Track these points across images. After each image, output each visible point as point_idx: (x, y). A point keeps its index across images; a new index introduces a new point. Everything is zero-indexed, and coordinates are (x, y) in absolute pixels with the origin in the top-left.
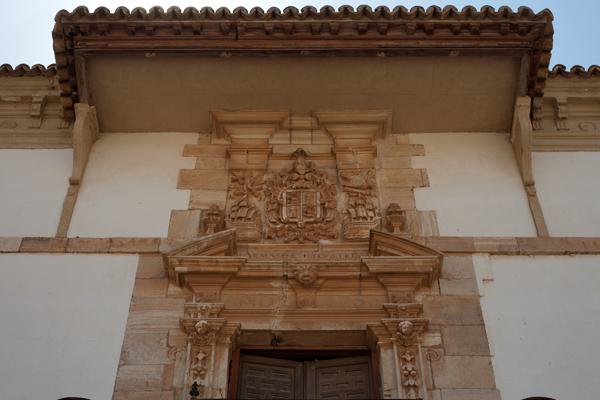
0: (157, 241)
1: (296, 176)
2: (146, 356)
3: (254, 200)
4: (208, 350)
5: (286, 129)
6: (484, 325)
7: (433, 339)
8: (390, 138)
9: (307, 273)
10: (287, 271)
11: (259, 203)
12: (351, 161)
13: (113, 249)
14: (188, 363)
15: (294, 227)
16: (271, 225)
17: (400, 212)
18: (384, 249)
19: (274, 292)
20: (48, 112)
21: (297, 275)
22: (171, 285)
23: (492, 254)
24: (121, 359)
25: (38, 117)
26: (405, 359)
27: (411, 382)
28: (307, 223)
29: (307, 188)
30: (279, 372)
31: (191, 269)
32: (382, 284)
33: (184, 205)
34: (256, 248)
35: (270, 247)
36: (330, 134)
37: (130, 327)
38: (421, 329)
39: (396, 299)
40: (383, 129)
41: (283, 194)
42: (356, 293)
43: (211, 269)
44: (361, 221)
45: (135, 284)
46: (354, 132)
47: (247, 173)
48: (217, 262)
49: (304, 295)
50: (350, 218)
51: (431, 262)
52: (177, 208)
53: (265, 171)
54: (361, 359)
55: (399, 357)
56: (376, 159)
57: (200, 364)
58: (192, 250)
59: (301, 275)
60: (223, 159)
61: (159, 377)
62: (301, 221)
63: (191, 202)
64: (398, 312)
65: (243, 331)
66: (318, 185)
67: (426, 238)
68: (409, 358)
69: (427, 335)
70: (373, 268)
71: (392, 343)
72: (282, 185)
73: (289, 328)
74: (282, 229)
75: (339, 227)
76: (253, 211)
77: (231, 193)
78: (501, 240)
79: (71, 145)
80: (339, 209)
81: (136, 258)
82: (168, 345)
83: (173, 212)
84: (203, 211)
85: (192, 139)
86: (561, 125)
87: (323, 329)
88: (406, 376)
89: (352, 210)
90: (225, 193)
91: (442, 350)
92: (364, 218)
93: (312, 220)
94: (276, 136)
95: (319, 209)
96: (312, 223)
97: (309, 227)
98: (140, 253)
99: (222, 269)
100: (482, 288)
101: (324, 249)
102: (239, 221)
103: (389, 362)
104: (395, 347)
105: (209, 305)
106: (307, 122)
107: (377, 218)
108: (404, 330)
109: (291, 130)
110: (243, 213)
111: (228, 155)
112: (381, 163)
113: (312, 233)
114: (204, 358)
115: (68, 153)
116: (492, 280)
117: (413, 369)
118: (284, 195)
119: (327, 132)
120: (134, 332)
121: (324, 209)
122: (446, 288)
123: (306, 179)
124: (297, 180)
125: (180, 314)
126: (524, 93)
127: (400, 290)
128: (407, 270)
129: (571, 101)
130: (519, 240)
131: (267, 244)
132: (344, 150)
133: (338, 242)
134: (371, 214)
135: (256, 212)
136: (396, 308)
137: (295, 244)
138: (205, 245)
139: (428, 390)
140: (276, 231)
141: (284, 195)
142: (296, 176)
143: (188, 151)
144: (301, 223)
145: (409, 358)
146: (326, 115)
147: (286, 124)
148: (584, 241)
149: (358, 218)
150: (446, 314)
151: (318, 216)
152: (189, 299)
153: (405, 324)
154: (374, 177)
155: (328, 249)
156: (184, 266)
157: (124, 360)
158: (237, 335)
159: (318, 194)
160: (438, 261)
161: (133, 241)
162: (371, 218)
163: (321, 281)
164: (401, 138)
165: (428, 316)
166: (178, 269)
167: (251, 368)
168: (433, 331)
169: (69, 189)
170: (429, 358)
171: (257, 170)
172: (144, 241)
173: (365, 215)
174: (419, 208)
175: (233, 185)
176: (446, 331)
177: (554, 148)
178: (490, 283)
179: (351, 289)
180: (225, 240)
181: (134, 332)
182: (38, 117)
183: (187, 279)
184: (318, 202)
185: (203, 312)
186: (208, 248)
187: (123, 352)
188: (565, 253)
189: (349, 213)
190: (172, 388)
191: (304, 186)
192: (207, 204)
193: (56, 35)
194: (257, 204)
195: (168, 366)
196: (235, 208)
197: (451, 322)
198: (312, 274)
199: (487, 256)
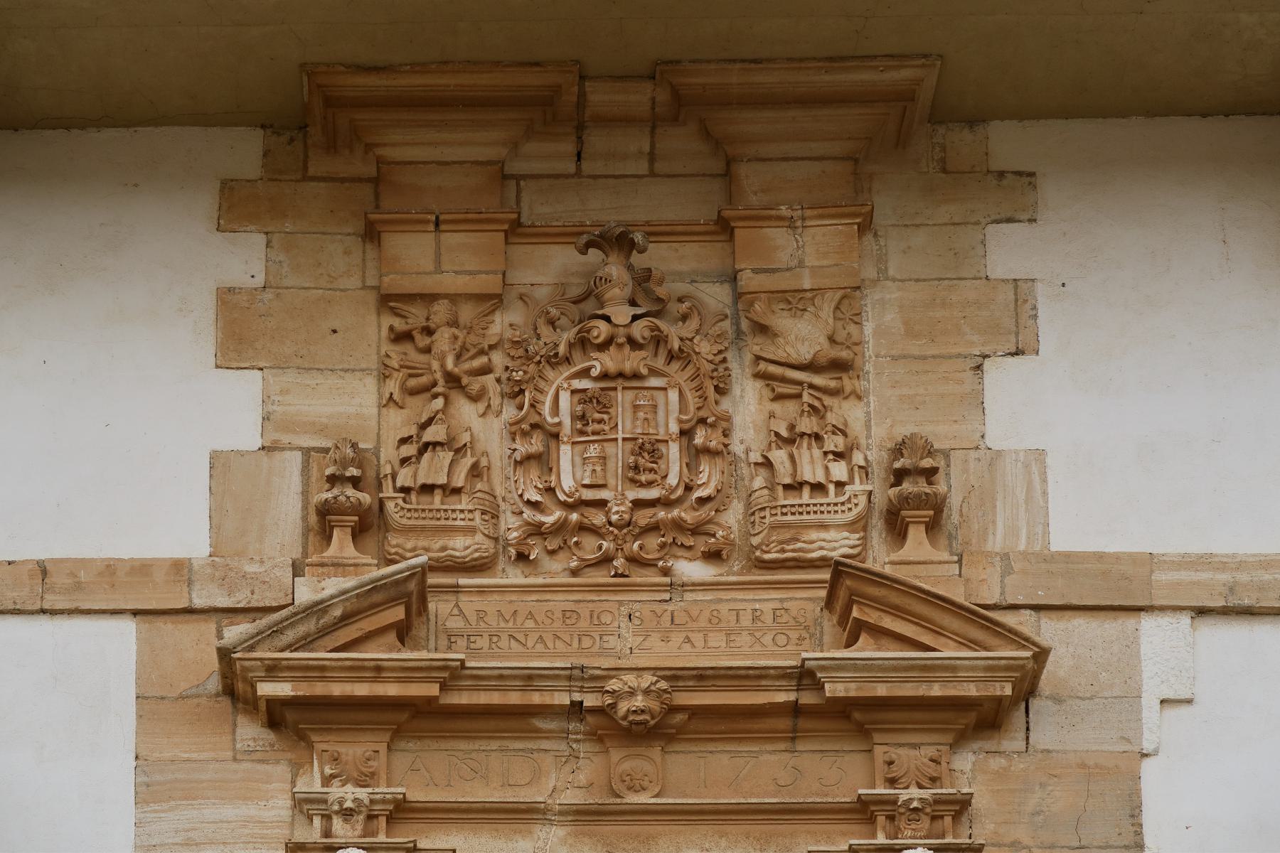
0: (180, 569)
3: (466, 412)
9: (639, 702)
15: (598, 518)
16: (528, 514)
17: (930, 474)
18: (872, 617)
19: (545, 744)
21: (613, 706)
22: (241, 719)
23: (1201, 612)
28: (638, 504)
29: (636, 376)
31: (304, 690)
34: (482, 591)
39: (895, 772)
44: (806, 496)
45: (139, 717)
47: (441, 311)
48: (379, 669)
50: (771, 487)
52: (225, 445)
53: (493, 301)
58: (301, 630)
59: (623, 707)
63: (266, 418)
67: (1005, 557)
72: (555, 361)
76: (468, 461)
77: (393, 386)
78: (1240, 564)
80: (737, 448)
81: (128, 627)
84: (307, 452)
89: (779, 456)
90: (371, 383)
92: (818, 488)
93: (653, 493)
94: (530, 147)
97: (643, 517)
98: (136, 613)
102: (425, 498)
105: (363, 794)
110: (434, 469)
113: (653, 541)
116: (1189, 702)
118: (565, 399)
119: (706, 134)
121: (695, 454)
125: (281, 807)
133: (732, 572)
134: (839, 470)
135: (475, 466)
136: (893, 801)
138: (337, 612)
140: (537, 530)
141: (565, 399)
144: (618, 511)
149: (795, 487)
151: (673, 480)
152: (297, 768)
154: (857, 319)
155: (700, 596)
156: (284, 679)
159: (673, 395)
162: (840, 485)
163: (679, 718)
166: (267, 689)
171: (412, 213)
172: (142, 569)
173: (820, 477)
175: (396, 354)
178: (1184, 710)
183: (290, 716)
184: (674, 428)
185: (347, 814)
186: (346, 619)
189: (767, 464)
191: (628, 367)
192: (322, 430)
194: (477, 424)
196: (408, 450)
198: (655, 705)
199: (1185, 620)
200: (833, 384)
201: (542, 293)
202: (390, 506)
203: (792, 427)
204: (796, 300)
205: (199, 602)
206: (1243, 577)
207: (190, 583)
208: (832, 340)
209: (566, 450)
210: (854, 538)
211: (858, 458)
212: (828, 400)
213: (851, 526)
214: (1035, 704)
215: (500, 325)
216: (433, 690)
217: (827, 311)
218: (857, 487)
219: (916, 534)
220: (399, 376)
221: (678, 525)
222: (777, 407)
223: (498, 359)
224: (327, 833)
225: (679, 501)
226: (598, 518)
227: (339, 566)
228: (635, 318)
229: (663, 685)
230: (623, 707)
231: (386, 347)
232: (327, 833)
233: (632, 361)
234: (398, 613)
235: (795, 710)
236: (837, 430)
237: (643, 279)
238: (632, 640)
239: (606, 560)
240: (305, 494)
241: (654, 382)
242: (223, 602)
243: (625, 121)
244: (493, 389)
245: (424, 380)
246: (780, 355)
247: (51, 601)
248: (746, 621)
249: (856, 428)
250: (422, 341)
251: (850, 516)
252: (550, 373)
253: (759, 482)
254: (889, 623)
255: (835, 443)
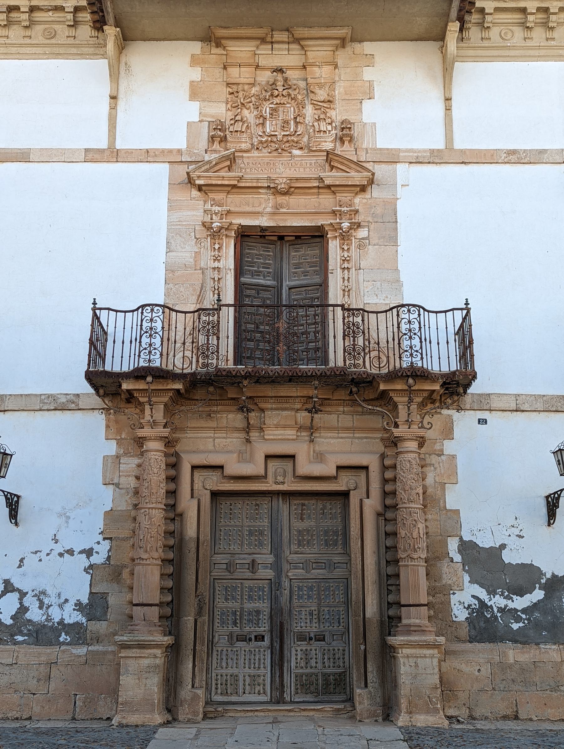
0: (179, 151)
1: (276, 93)
2: (182, 246)
3: (246, 112)
4: (221, 241)
5: (268, 42)
6: (397, 222)
7: (362, 233)
8: (349, 49)
9: (283, 186)
10: (270, 183)
11: (249, 115)
12: (317, 75)
13: (150, 159)
14: (210, 251)
19: (262, 196)
20: (80, 19)
22: (193, 189)
24: (167, 248)
25: (72, 26)
26: (343, 248)
27: (346, 265)
29: (284, 104)
30: (265, 247)
32: (333, 192)
33: (196, 118)
34: (248, 157)
35: (259, 157)
36: (303, 47)
37: (170, 224)
38: (355, 227)
40: (343, 43)
41: (267, 108)
42: (316, 197)
43: (219, 182)
46: (322, 45)
47: (240, 87)
49: (281, 199)
50: (314, 131)
51: (366, 177)
54: (318, 240)
55: (340, 247)
56: (337, 70)
57: (217, 253)
59: (279, 187)
60: (221, 70)
61: (192, 260)
62: (280, 134)
64: (341, 213)
65: (242, 226)
66: (292, 99)
67: (367, 149)
68: (346, 248)
69: (359, 229)
70: (327, 182)
71: (336, 237)
72: (265, 100)
73: (272, 224)
74: (266, 141)
75: (305, 139)
77: (229, 106)
79: (104, 56)
81: (167, 165)
82: (195, 238)
83: (188, 123)
84: (209, 122)
85: (196, 47)
86: (485, 34)
87: (294, 225)
88: (343, 260)
89: (316, 124)
90: (224, 105)
91: (368, 241)
93: (288, 133)
95: (292, 122)
96: (287, 135)
98: (169, 162)
99: (226, 183)
100: (400, 191)
101: (295, 159)
103: (334, 246)
104: (338, 240)
105: (220, 209)
106: (284, 36)
107: (334, 132)
108: (344, 230)
109: (272, 43)
110: (238, 126)
111: (225, 68)
112: (340, 75)
113: (287, 145)
114: (219, 248)
115: (102, 65)
117: (348, 256)
118: (268, 109)
120: (173, 227)
121: (297, 123)
122: (375, 192)
123: (283, 95)
124: (276, 97)
125: (200, 213)
126: (454, 19)
127: (344, 197)
128: (350, 183)
129: (497, 9)
130: (432, 151)
131: (255, 153)
132: (313, 65)
134: (329, 128)
137: (275, 154)
138: (214, 163)
139: (356, 270)
140: (261, 142)
141: (268, 109)
142: (276, 93)
143: (195, 61)
145: (346, 248)
146: (300, 32)
147: (269, 39)
148: (478, 152)
149: (320, 131)
150: (373, 214)
151: (292, 130)
153: (346, 225)
154: (334, 90)
155: (298, 159)
157: (169, 250)
158: (238, 228)
159: (292, 109)
160: (371, 177)
161: (163, 151)
163: (293, 189)
164: (357, 46)
165: (360, 218)
166: (198, 182)
167: (248, 246)
168: (364, 227)
169: (110, 103)
170: (359, 247)
172: (170, 151)
174: (364, 120)
176: (372, 227)
177: (476, 59)
178: (407, 187)
179: (313, 194)
180: (227, 158)
181: (173, 227)
182: (72, 26)
183: (204, 188)
184: (292, 117)
185: (216, 214)
187: (168, 243)
188: (463, 163)
189: (313, 126)
190: (201, 269)
191: (282, 102)
192: (213, 117)
193: (85, 372)
194: (248, 115)
195: (196, 252)
196: (232, 122)
197: (376, 220)
200: (328, 106)
201: (264, 83)
202: (228, 136)
203: (319, 117)
204: (321, 86)
205: (183, 160)
206: (420, 155)
207: (182, 155)
208: (328, 95)
209: (268, 122)
210: (333, 145)
211: (334, 125)
212: (327, 110)
213: (332, 142)
214: (373, 186)
215: (254, 90)
216: (236, 183)
217: (327, 88)
218: (334, 132)
219: (346, 143)
220: (231, 103)
221: (293, 141)
222: (316, 112)
223: (253, 99)
224: (212, 219)
225: (294, 135)
226: (275, 140)
227: (215, 151)
228: (284, 90)
229: (288, 181)
230: (279, 187)
231: (228, 96)
232: (212, 219)
233: (284, 100)
234: (228, 163)
235: (319, 187)
236: (329, 118)
237: (286, 80)
238: (282, 170)
239: (277, 150)
240: (209, 132)
241: (288, 105)
242: (189, 160)
243: (283, 42)
244: (252, 107)
245: (236, 104)
246: (316, 99)
247: (150, 159)
248: (308, 165)
249: (334, 117)
250: (236, 95)
251: (332, 139)
252: (265, 103)
253: (311, 131)
254: (339, 166)
255: (329, 121)
